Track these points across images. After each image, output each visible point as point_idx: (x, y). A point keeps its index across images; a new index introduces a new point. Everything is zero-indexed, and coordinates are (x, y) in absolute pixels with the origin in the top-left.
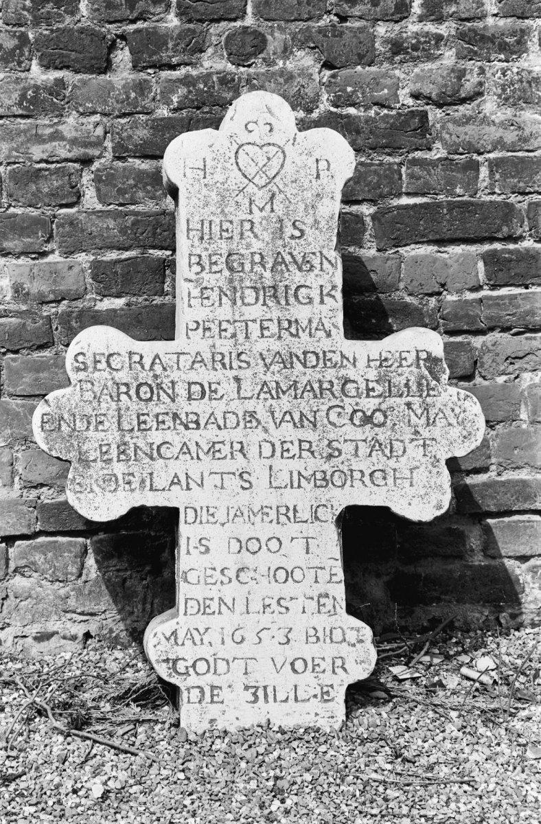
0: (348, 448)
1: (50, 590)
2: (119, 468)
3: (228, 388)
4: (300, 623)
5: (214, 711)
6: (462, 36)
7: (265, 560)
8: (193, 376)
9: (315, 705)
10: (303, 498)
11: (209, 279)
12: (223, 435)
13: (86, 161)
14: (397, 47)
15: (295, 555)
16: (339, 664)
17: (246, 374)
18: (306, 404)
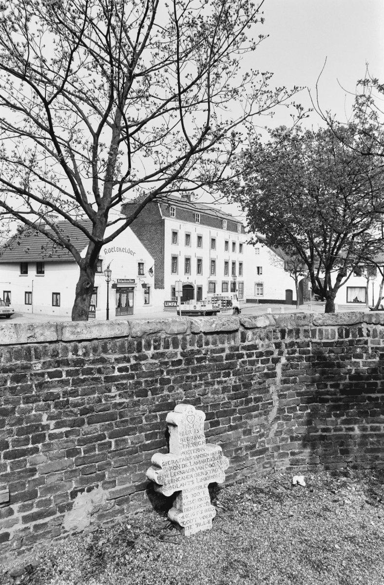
0: (209, 472)
1: (137, 503)
2: (171, 485)
3: (189, 464)
4: (204, 508)
5: (191, 531)
6: (205, 383)
7: (197, 497)
8: (183, 463)
9: (208, 525)
10: (202, 484)
11: (184, 443)
12: (188, 474)
13: (144, 415)
14: (195, 386)
15: (202, 495)
16: (211, 515)
17: (191, 461)
18: (202, 465)
